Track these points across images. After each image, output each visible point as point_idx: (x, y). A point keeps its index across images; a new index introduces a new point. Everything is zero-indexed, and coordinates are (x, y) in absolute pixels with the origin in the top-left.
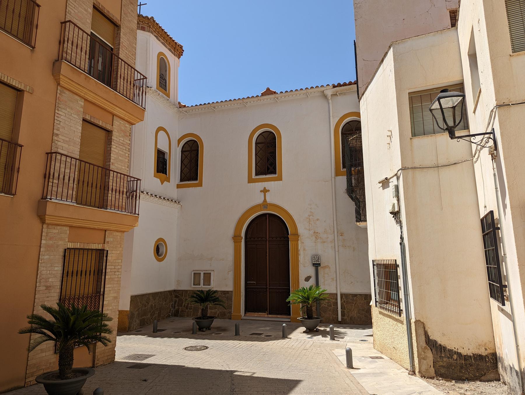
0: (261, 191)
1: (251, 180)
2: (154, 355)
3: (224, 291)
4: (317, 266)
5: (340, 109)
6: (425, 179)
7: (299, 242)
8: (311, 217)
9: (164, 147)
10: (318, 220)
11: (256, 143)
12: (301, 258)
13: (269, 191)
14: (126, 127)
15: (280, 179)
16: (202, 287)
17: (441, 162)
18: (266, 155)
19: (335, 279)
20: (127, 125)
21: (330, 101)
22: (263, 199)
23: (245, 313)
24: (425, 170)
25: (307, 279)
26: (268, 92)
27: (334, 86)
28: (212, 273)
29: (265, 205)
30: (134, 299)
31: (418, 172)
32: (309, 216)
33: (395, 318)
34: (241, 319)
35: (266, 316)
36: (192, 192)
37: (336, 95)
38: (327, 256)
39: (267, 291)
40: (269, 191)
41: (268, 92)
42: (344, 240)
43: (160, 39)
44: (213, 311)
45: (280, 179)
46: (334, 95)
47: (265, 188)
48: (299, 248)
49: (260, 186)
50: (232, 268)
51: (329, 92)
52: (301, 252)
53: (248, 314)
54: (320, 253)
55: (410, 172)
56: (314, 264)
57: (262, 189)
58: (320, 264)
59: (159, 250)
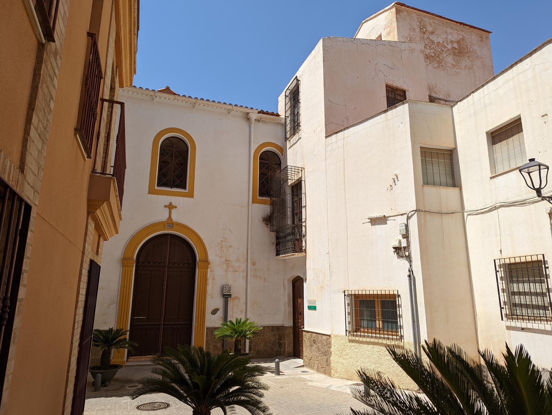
1: (151, 191)
2: (352, 410)
4: (226, 297)
5: (265, 135)
6: (433, 221)
7: (209, 270)
8: (224, 243)
10: (231, 246)
12: (209, 288)
13: (176, 207)
15: (191, 195)
17: (444, 210)
18: (174, 165)
19: (244, 311)
21: (252, 126)
23: (128, 358)
24: (433, 214)
25: (214, 312)
26: (167, 91)
27: (259, 112)
31: (428, 215)
32: (222, 241)
33: (370, 342)
37: (259, 121)
38: (238, 287)
40: (176, 207)
41: (167, 91)
42: (256, 270)
45: (191, 195)
46: (258, 121)
47: (171, 203)
48: (208, 277)
49: (166, 199)
51: (254, 116)
52: (210, 282)
53: (132, 359)
54: (230, 283)
55: (422, 214)
56: (224, 295)
57: (168, 204)
58: (231, 295)
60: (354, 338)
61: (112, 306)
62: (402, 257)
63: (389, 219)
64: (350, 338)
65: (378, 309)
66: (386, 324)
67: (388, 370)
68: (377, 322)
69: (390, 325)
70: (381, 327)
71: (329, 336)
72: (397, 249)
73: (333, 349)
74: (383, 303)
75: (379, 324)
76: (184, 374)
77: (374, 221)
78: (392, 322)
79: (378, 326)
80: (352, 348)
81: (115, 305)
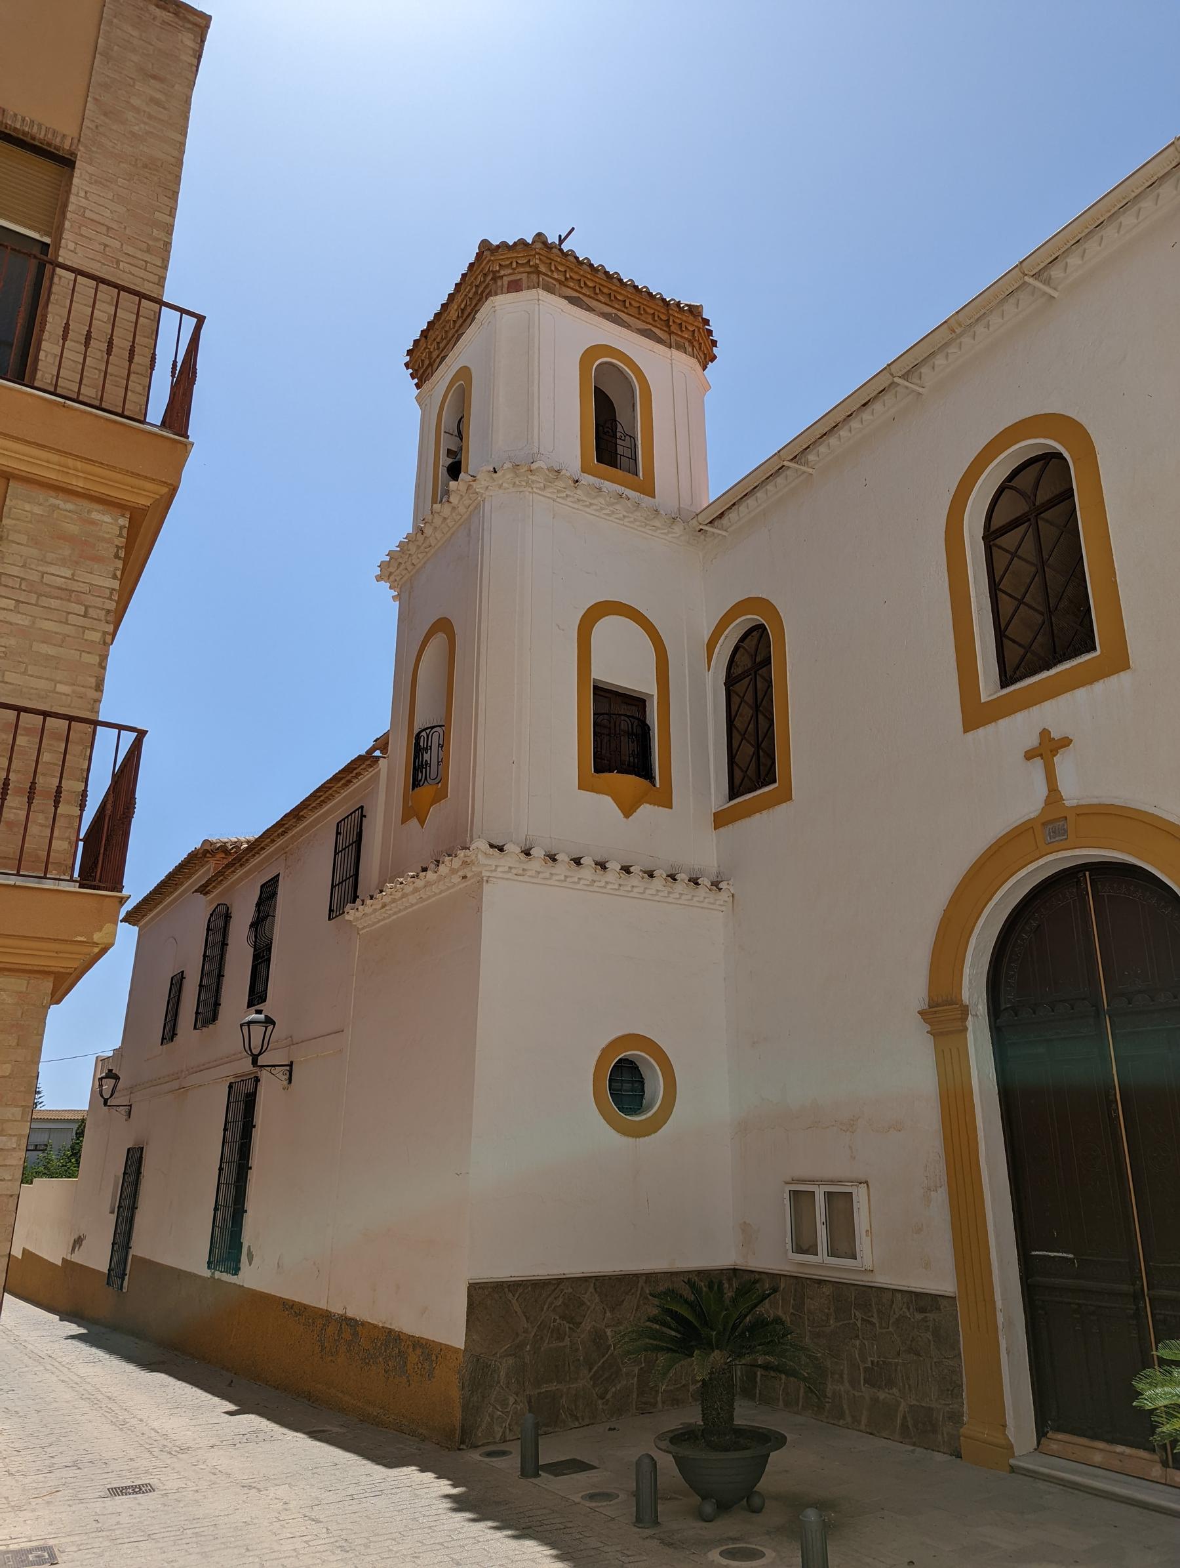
0: (1029, 755)
3: (918, 1295)
9: (624, 664)
11: (991, 536)
13: (1066, 742)
14: (93, 523)
16: (822, 1266)
20: (95, 516)
22: (1042, 791)
23: (1041, 1434)
28: (860, 1197)
29: (1055, 821)
30: (485, 1299)
34: (1013, 1469)
35: (1157, 1471)
36: (766, 825)
39: (1138, 1314)
40: (1066, 742)
43: (593, 304)
44: (882, 1395)
47: (1045, 733)
49: (1020, 729)
50: (939, 1169)
53: (1058, 1440)
57: (1033, 741)
59: (627, 1084)
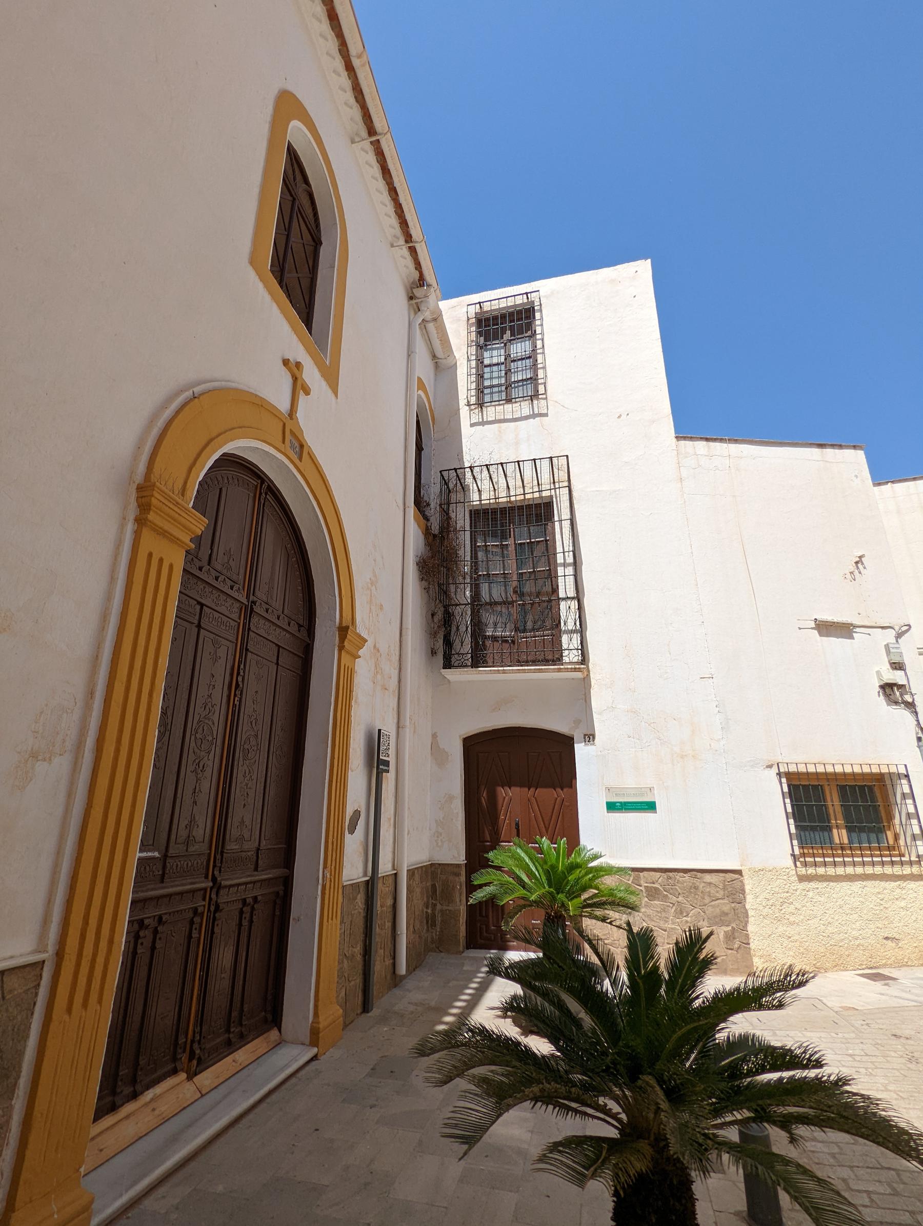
60: (811, 871)
61: (41, 767)
62: (896, 703)
63: (857, 630)
64: (802, 871)
65: (834, 803)
66: (854, 835)
67: (906, 929)
68: (835, 831)
69: (864, 836)
70: (846, 841)
71: (739, 872)
72: (888, 688)
73: (750, 902)
74: (842, 789)
75: (840, 835)
76: (791, 1073)
77: (826, 628)
78: (871, 830)
79: (837, 841)
80: (811, 894)
81: (61, 764)
